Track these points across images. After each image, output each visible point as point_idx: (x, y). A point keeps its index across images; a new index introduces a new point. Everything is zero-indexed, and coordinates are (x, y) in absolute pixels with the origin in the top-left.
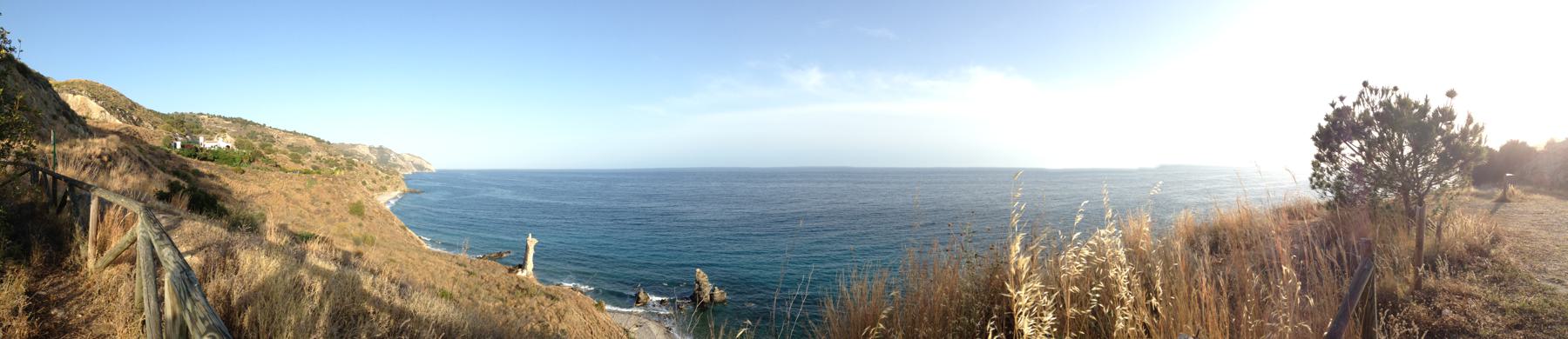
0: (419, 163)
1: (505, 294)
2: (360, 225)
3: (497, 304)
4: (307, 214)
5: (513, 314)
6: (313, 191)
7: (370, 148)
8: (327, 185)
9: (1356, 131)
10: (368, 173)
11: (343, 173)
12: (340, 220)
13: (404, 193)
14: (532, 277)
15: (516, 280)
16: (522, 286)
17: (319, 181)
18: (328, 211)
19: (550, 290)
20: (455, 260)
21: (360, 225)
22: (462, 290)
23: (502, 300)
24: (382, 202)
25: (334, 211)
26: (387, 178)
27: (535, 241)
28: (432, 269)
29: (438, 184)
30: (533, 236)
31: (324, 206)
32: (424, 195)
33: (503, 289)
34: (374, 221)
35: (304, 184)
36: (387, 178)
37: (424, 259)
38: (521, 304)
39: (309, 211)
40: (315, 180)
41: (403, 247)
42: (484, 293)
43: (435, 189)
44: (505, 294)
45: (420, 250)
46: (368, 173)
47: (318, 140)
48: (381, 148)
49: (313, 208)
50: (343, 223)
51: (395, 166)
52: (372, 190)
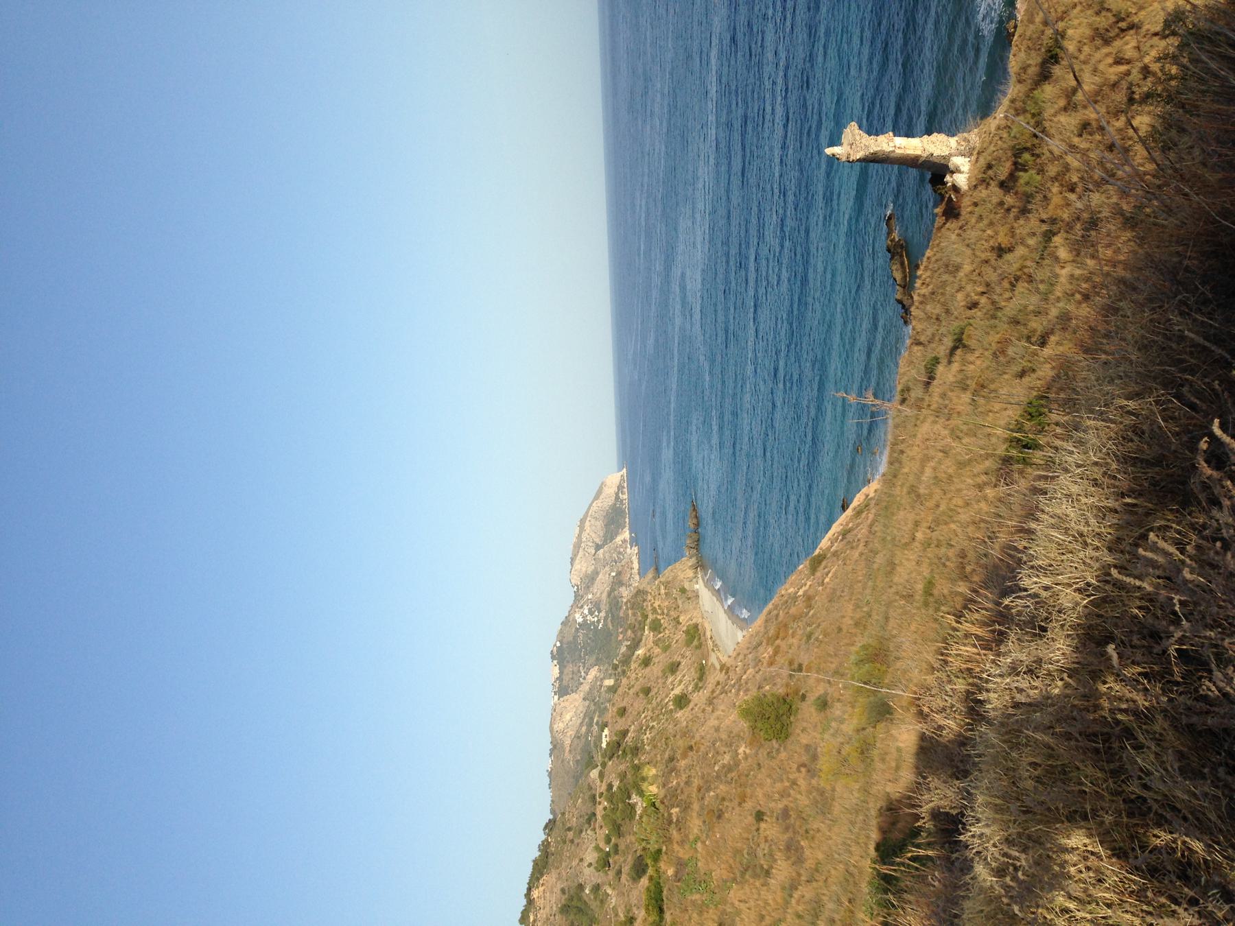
0: (599, 524)
1: (1030, 226)
2: (823, 704)
3: (1063, 254)
4: (806, 892)
5: (1096, 198)
6: (719, 873)
7: (563, 690)
8: (695, 825)
9: (648, 905)
10: (647, 691)
11: (650, 772)
12: (812, 773)
13: (701, 565)
14: (974, 137)
15: (983, 193)
16: (1003, 171)
17: (682, 853)
18: (786, 813)
19: (1024, 69)
20: (917, 392)
21: (823, 704)
22: (1016, 368)
23: (1048, 236)
24: (740, 636)
25: (784, 794)
26: (656, 627)
27: (852, 132)
28: (948, 466)
29: (667, 454)
30: (835, 140)
31: (770, 829)
32: (706, 509)
33: (1012, 232)
34: (804, 659)
35: (702, 909)
36: (656, 627)
37: (913, 490)
38: (1067, 168)
39: (793, 887)
40: (681, 865)
41: (880, 560)
42: (1024, 298)
43: (683, 461)
44: (1030, 226)
45: (885, 506)
46: (647, 691)
47: (540, 867)
48: (560, 656)
49: (782, 870)
50: (824, 764)
51: (614, 603)
52: (702, 672)
